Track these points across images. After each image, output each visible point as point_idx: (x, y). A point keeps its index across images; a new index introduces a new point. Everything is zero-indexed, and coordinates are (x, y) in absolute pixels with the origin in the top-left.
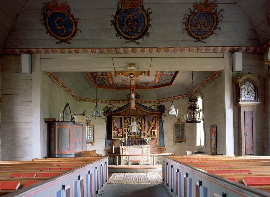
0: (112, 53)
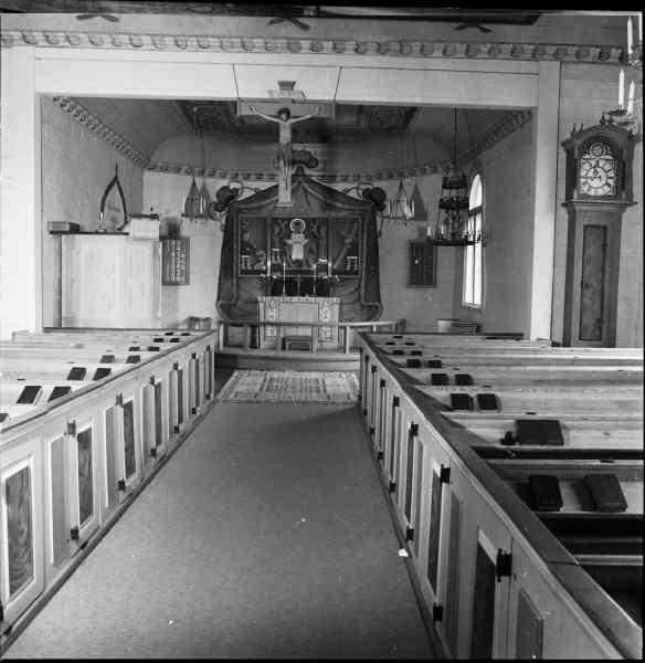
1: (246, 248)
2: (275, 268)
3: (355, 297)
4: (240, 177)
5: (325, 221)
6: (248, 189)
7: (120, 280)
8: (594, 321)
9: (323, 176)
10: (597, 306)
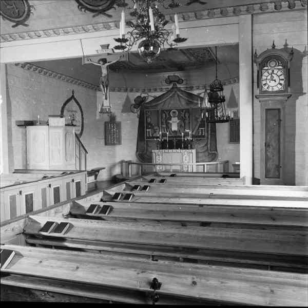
0: (281, 10)
1: (150, 125)
2: (164, 135)
3: (206, 148)
4: (146, 91)
5: (187, 111)
6: (151, 96)
7: (50, 147)
8: (274, 166)
9: (187, 87)
10: (276, 158)
